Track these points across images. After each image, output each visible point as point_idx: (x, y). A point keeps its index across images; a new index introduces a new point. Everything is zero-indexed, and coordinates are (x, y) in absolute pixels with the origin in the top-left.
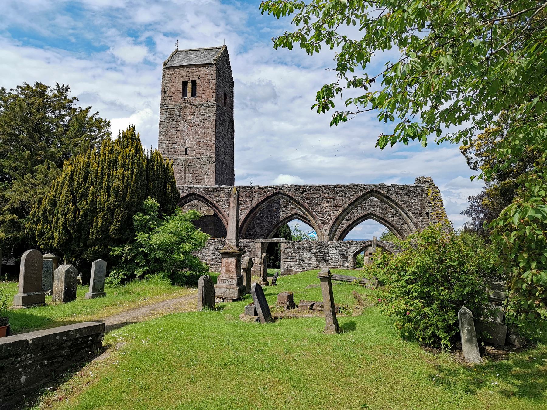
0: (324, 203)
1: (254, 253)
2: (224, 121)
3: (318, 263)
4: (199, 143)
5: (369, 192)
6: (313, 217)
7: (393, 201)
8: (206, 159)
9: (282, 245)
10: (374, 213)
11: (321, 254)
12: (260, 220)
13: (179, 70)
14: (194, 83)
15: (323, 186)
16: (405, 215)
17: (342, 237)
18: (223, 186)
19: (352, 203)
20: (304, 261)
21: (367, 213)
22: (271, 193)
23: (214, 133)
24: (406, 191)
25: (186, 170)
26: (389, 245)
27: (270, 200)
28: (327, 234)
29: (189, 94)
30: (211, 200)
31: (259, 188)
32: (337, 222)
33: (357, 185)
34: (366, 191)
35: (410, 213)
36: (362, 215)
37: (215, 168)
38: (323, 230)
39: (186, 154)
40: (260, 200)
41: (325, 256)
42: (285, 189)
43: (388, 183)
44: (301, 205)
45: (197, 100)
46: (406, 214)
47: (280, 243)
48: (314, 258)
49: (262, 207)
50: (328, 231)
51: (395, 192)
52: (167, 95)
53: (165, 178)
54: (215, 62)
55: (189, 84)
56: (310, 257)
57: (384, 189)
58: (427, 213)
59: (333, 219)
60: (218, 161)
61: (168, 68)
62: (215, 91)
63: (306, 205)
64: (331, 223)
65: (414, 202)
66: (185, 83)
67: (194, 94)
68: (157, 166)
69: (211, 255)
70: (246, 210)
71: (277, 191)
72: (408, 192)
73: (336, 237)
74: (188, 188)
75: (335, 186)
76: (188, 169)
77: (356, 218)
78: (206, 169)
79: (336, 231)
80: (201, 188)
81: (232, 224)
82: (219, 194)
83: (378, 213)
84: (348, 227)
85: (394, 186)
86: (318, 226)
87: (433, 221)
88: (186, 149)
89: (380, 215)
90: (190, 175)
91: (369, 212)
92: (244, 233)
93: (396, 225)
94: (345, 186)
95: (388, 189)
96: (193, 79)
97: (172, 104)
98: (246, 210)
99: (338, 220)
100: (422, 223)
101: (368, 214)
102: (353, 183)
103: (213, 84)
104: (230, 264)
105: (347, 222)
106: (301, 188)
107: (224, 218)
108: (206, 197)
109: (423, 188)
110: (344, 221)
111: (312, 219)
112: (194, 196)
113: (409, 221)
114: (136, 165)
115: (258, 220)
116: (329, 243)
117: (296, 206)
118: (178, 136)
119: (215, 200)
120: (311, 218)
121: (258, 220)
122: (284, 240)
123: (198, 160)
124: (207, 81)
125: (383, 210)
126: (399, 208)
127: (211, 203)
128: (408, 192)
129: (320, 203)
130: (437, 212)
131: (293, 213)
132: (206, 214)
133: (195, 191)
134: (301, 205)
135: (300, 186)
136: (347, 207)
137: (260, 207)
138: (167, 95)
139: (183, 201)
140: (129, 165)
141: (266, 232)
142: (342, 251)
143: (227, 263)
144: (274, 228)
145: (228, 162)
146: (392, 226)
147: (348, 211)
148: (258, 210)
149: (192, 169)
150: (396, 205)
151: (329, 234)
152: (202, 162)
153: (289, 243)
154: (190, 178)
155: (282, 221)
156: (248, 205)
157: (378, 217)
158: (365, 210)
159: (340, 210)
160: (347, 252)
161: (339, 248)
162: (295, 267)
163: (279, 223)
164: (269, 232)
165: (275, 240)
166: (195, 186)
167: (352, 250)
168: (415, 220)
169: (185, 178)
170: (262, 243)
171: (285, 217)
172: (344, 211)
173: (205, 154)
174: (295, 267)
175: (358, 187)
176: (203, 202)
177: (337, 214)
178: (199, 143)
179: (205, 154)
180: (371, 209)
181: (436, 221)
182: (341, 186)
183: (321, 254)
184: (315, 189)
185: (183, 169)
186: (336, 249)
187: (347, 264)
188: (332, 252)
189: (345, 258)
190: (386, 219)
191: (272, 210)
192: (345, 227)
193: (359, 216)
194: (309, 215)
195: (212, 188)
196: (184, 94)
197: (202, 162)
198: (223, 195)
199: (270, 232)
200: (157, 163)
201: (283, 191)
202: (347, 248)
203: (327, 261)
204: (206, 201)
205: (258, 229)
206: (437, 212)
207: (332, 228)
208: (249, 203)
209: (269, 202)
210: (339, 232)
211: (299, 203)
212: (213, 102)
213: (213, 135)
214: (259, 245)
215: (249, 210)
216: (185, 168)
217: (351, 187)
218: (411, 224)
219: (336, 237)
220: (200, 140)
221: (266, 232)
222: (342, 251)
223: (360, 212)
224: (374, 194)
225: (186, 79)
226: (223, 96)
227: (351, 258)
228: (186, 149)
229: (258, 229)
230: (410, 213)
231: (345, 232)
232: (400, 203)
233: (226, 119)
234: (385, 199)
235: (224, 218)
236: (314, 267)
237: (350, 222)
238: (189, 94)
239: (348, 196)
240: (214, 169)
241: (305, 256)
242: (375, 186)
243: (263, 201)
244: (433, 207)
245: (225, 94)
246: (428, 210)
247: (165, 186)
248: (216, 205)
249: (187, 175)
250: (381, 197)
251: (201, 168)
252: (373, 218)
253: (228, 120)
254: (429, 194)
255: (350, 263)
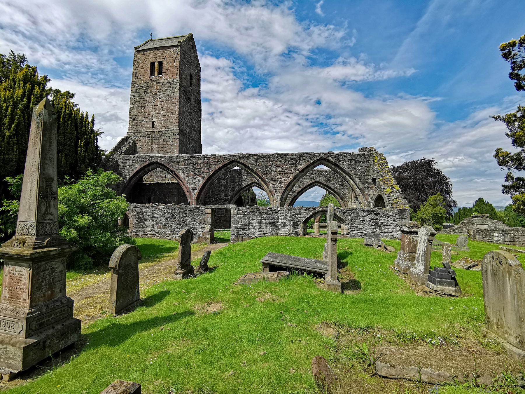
0: (276, 171)
1: (204, 220)
2: (189, 99)
3: (268, 229)
4: (164, 117)
5: (318, 160)
6: (266, 184)
7: (340, 168)
8: (170, 132)
9: (232, 211)
10: (320, 181)
11: (271, 221)
12: (224, 188)
13: (148, 52)
14: (160, 63)
15: (276, 154)
16: (352, 182)
17: (291, 204)
18: (182, 155)
19: (302, 171)
20: (254, 227)
21: (314, 181)
22: (227, 162)
23: (178, 107)
24: (353, 157)
25: (152, 142)
26: (341, 211)
27: (226, 168)
28: (279, 200)
29: (156, 73)
30: (171, 168)
31: (216, 157)
32: (289, 188)
33: (308, 153)
34: (316, 159)
35: (357, 180)
36: (310, 183)
37: (178, 140)
38: (275, 196)
39: (153, 127)
40: (217, 168)
41: (275, 222)
42: (240, 157)
43: (337, 152)
44: (255, 173)
45: (163, 79)
46: (353, 180)
47: (228, 211)
48: (263, 225)
49: (219, 175)
50: (279, 197)
51: (343, 159)
52: (137, 75)
53: (78, 133)
54: (179, 44)
55: (156, 65)
56: (260, 223)
57: (333, 157)
58: (374, 180)
59: (284, 185)
60: (182, 133)
61: (139, 52)
62: (179, 70)
63: (260, 173)
64: (283, 189)
65: (361, 169)
66: (153, 64)
67: (160, 73)
68: (64, 118)
69: (161, 222)
70: (204, 177)
71: (232, 159)
72: (355, 160)
73: (288, 202)
74: (150, 157)
75: (286, 155)
76: (154, 141)
77: (305, 186)
78: (171, 141)
79: (287, 196)
80: (162, 157)
81: (29, 185)
82: (178, 163)
83: (324, 181)
84: (298, 193)
85: (342, 154)
86: (271, 192)
87: (382, 187)
88: (153, 122)
89: (325, 183)
90: (156, 146)
91: (316, 180)
92: (203, 199)
93: (338, 191)
94: (296, 155)
95: (337, 157)
96: (160, 60)
97: (142, 82)
98: (204, 177)
99: (289, 187)
100: (367, 189)
101: (315, 182)
102: (303, 151)
103: (177, 64)
104: (19, 280)
105: (297, 188)
106: (255, 157)
107: (184, 185)
108: (167, 165)
109: (369, 156)
110: (295, 188)
111: (265, 186)
112: (156, 165)
113: (355, 187)
114: (19, 111)
115: (223, 188)
116: (279, 209)
117: (250, 174)
118: (146, 111)
119: (175, 168)
120: (264, 185)
121: (223, 188)
122: (235, 206)
123: (164, 132)
124: (172, 61)
125: (327, 179)
126: (347, 174)
127: (172, 171)
128: (355, 160)
129: (273, 171)
130: (385, 178)
131: (252, 181)
132: (171, 182)
133: (156, 160)
134: (255, 173)
135: (254, 155)
136: (298, 175)
137: (217, 175)
138: (137, 75)
139: (146, 169)
140: (7, 110)
141: (229, 197)
142: (293, 218)
143: (12, 278)
144: (236, 195)
145: (194, 137)
146: (335, 192)
147: (298, 178)
148: (215, 178)
149: (158, 141)
150: (344, 172)
151: (281, 200)
152: (167, 135)
153: (239, 210)
154: (156, 149)
155: (243, 188)
156: (207, 172)
157: (323, 184)
158: (312, 179)
159: (291, 177)
160: (297, 219)
161: (289, 215)
162: (245, 233)
163: (240, 190)
164: (232, 197)
165: (225, 206)
166: (156, 155)
167: (303, 216)
168: (361, 186)
169: (152, 149)
170: (212, 209)
171: (245, 185)
172: (294, 178)
173: (169, 127)
174: (245, 233)
175: (308, 155)
176: (164, 170)
177: (288, 181)
178: (164, 117)
179: (169, 127)
180: (318, 178)
181: (385, 186)
182: (292, 155)
183: (271, 221)
184: (267, 157)
185: (150, 141)
186: (286, 215)
187: (297, 230)
188: (281, 218)
189: (295, 224)
190: (330, 186)
191: (235, 179)
192: (296, 193)
193: (307, 184)
194: (262, 182)
195: (172, 157)
196: (152, 73)
197: (167, 135)
198: (182, 164)
199: (233, 197)
200: (64, 114)
201: (238, 160)
202: (297, 214)
203: (277, 227)
204: (167, 169)
205: (223, 196)
206: (385, 178)
207: (283, 194)
208: (206, 171)
209: (226, 170)
210: (289, 197)
211: (253, 171)
212: (177, 80)
213: (177, 110)
214: (209, 211)
215: (206, 177)
216: (152, 140)
217: (301, 155)
218: (357, 190)
219: (288, 202)
220: (165, 114)
221: (229, 197)
222: (293, 218)
223: (308, 181)
224: (323, 161)
225: (153, 60)
226: (188, 76)
227: (301, 225)
228: (153, 122)
229: (223, 196)
230: (357, 180)
231: (295, 198)
232: (347, 170)
233: (192, 97)
234: (333, 166)
235: (184, 185)
236: (264, 234)
237: (300, 189)
238: (156, 73)
239: (299, 164)
240: (177, 141)
241: (256, 222)
242: (324, 154)
243: (220, 169)
244: (380, 173)
245: (191, 76)
246: (376, 176)
247: (76, 146)
248: (176, 173)
249: (153, 146)
250: (330, 164)
251: (166, 140)
252: (319, 186)
253: (194, 99)
254: (376, 161)
255: (300, 230)
